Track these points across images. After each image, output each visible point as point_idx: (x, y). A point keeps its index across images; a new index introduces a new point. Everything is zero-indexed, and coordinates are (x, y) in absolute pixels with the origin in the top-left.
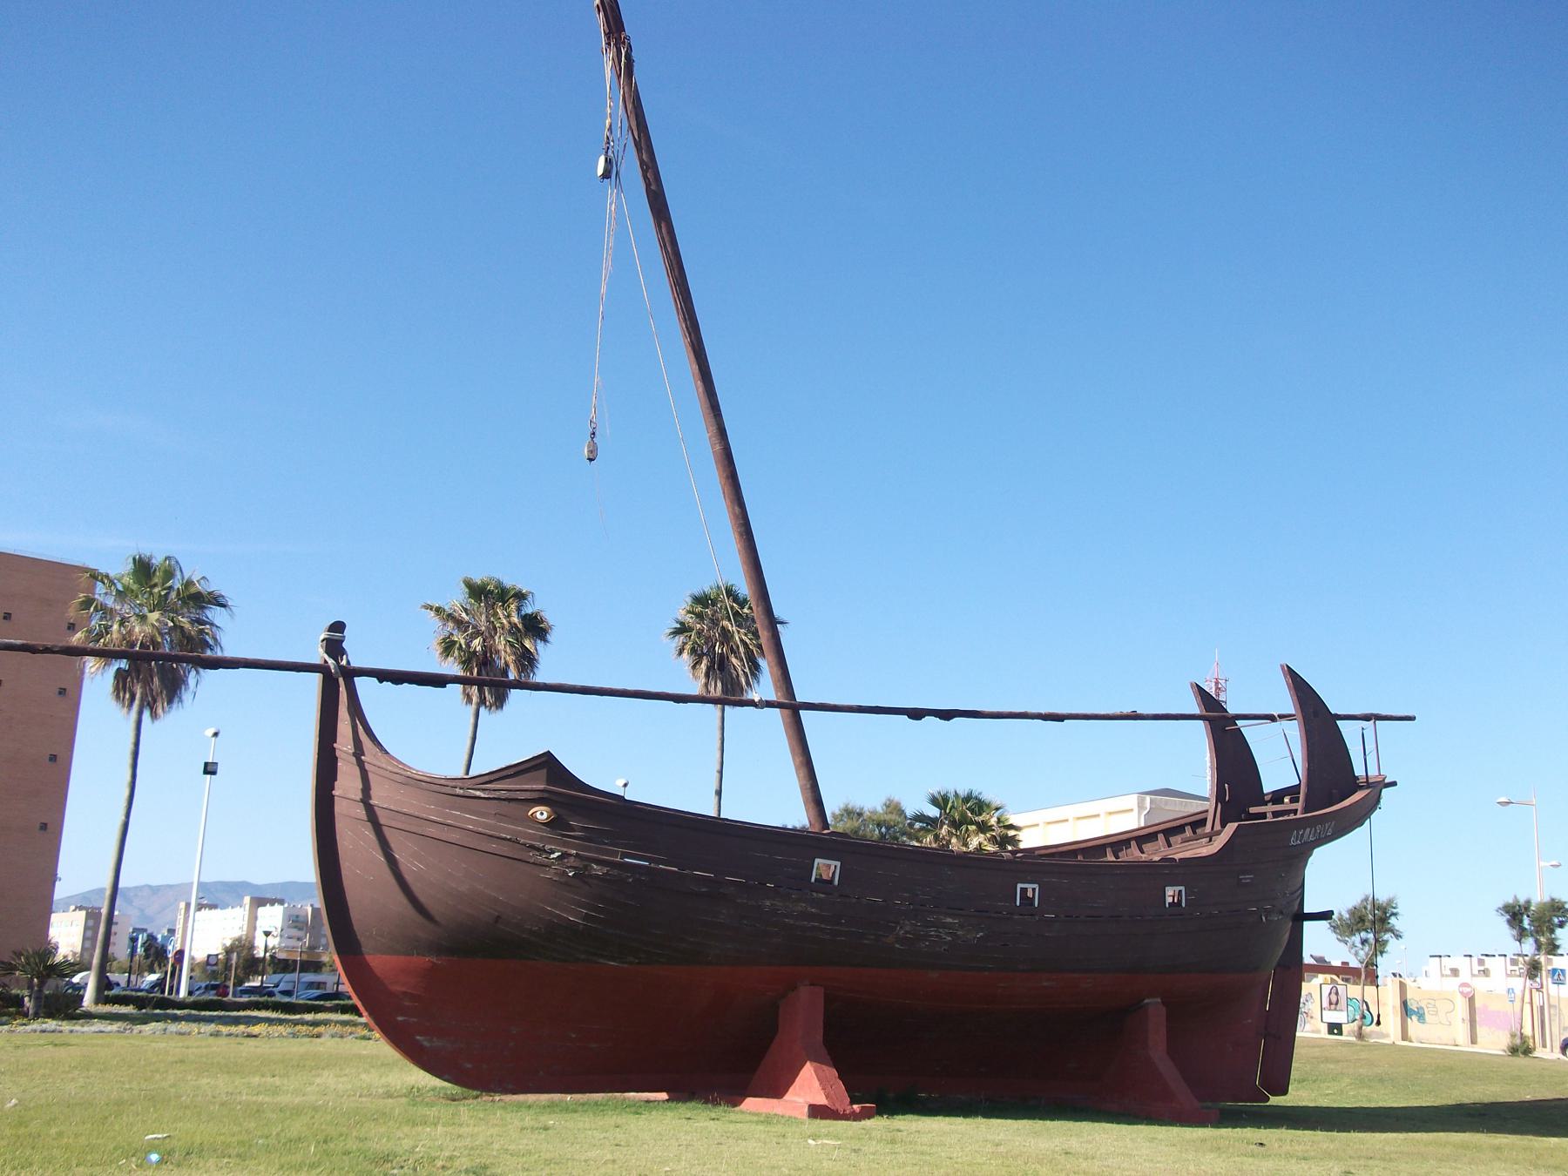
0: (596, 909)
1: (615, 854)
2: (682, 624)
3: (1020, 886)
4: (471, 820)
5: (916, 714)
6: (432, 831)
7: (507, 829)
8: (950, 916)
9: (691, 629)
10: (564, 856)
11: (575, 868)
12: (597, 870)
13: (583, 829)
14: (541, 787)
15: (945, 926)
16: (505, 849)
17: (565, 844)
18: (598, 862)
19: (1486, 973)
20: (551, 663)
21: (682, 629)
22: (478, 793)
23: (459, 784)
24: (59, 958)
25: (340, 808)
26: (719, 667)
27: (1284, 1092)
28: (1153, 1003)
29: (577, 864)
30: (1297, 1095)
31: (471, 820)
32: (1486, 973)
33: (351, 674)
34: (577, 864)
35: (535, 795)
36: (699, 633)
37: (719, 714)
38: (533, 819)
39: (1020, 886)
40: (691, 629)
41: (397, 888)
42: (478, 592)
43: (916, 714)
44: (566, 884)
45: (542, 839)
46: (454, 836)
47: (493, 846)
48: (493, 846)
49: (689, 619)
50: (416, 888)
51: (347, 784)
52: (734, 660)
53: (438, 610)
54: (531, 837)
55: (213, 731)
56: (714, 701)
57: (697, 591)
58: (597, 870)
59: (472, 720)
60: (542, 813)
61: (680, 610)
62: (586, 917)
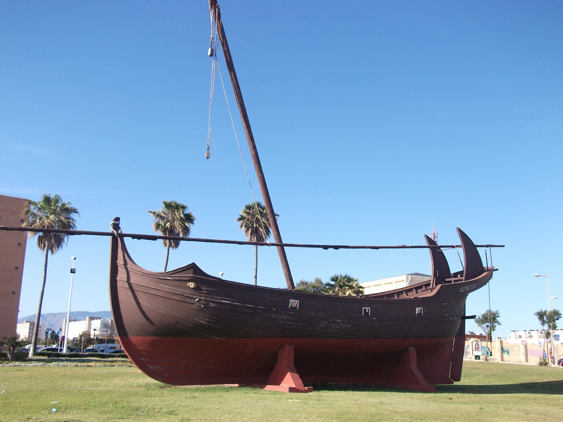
0: (213, 319)
1: (218, 299)
2: (242, 216)
4: (166, 288)
5: (326, 247)
6: (152, 292)
7: (180, 291)
8: (339, 319)
10: (200, 300)
11: (204, 304)
12: (212, 305)
15: (337, 323)
16: (178, 298)
17: (201, 296)
18: (212, 302)
19: (531, 337)
21: (242, 218)
22: (169, 278)
25: (119, 284)
26: (255, 232)
28: (412, 349)
29: (205, 303)
30: (464, 381)
31: (166, 288)
32: (531, 337)
33: (122, 236)
34: (205, 303)
35: (189, 278)
36: (248, 220)
38: (189, 287)
42: (168, 206)
43: (326, 247)
44: (200, 310)
45: (192, 294)
46: (160, 294)
47: (174, 297)
48: (174, 297)
50: (147, 313)
51: (122, 275)
53: (154, 213)
54: (188, 293)
58: (212, 305)
60: (192, 285)
62: (208, 322)
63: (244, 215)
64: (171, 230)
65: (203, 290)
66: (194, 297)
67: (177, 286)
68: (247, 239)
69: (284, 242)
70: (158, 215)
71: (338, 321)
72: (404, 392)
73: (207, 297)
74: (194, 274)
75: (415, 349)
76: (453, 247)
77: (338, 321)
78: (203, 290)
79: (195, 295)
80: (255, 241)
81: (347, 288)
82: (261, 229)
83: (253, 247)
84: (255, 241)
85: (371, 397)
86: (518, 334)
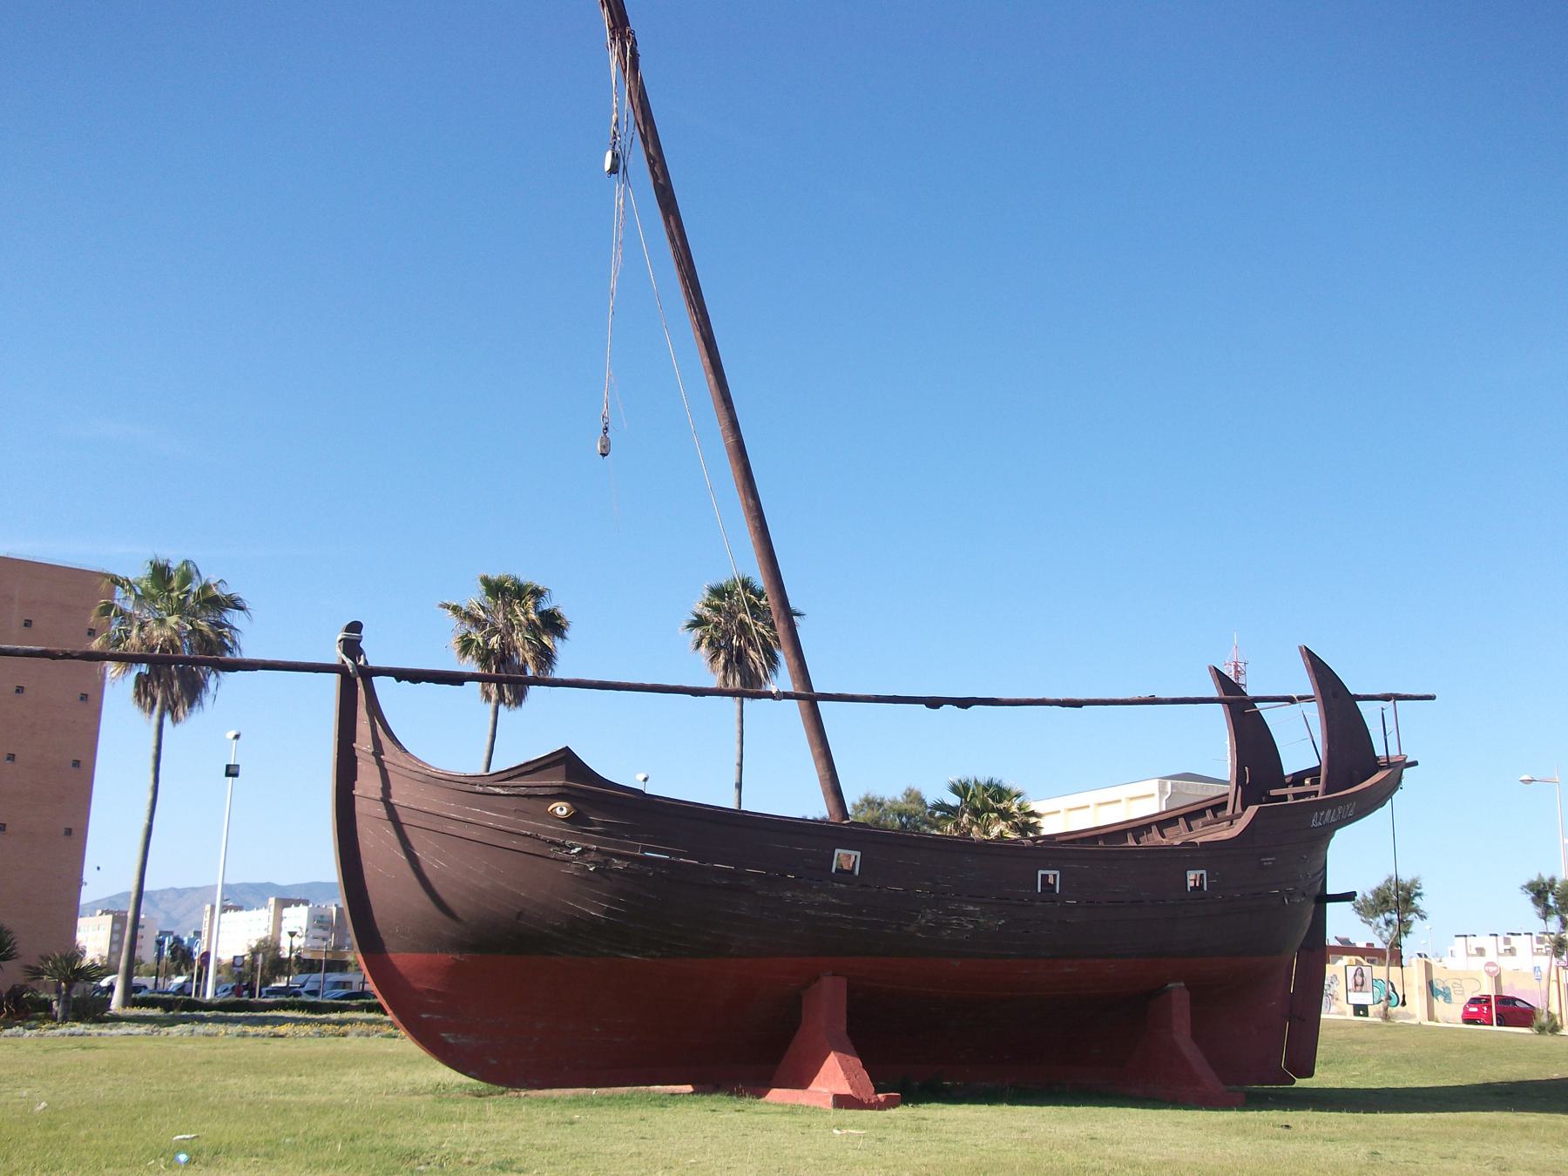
0: (619, 904)
1: (635, 848)
2: (698, 616)
4: (491, 817)
5: (934, 703)
6: (452, 828)
7: (529, 825)
8: (974, 904)
11: (595, 863)
13: (603, 824)
14: (561, 782)
15: (966, 914)
17: (586, 840)
19: (1512, 951)
20: (569, 659)
21: (699, 622)
22: (497, 790)
23: (478, 781)
24: (86, 962)
26: (737, 660)
27: (1310, 1074)
29: (599, 858)
30: (1324, 1077)
31: (491, 817)
32: (1512, 951)
33: (369, 673)
34: (599, 858)
35: (555, 791)
38: (553, 815)
42: (495, 589)
43: (934, 703)
44: (587, 879)
45: (562, 834)
46: (474, 833)
47: (514, 843)
48: (514, 843)
51: (367, 783)
52: (752, 653)
53: (456, 609)
54: (552, 833)
56: (733, 694)
57: (714, 584)
59: (491, 718)
60: (561, 809)
61: (697, 603)
62: (608, 912)
63: (707, 613)
65: (592, 824)
66: (568, 843)
68: (714, 681)
74: (568, 778)
75: (1187, 987)
76: (1291, 700)
78: (592, 824)
79: (570, 836)
80: (738, 685)
83: (731, 703)
86: (1474, 943)
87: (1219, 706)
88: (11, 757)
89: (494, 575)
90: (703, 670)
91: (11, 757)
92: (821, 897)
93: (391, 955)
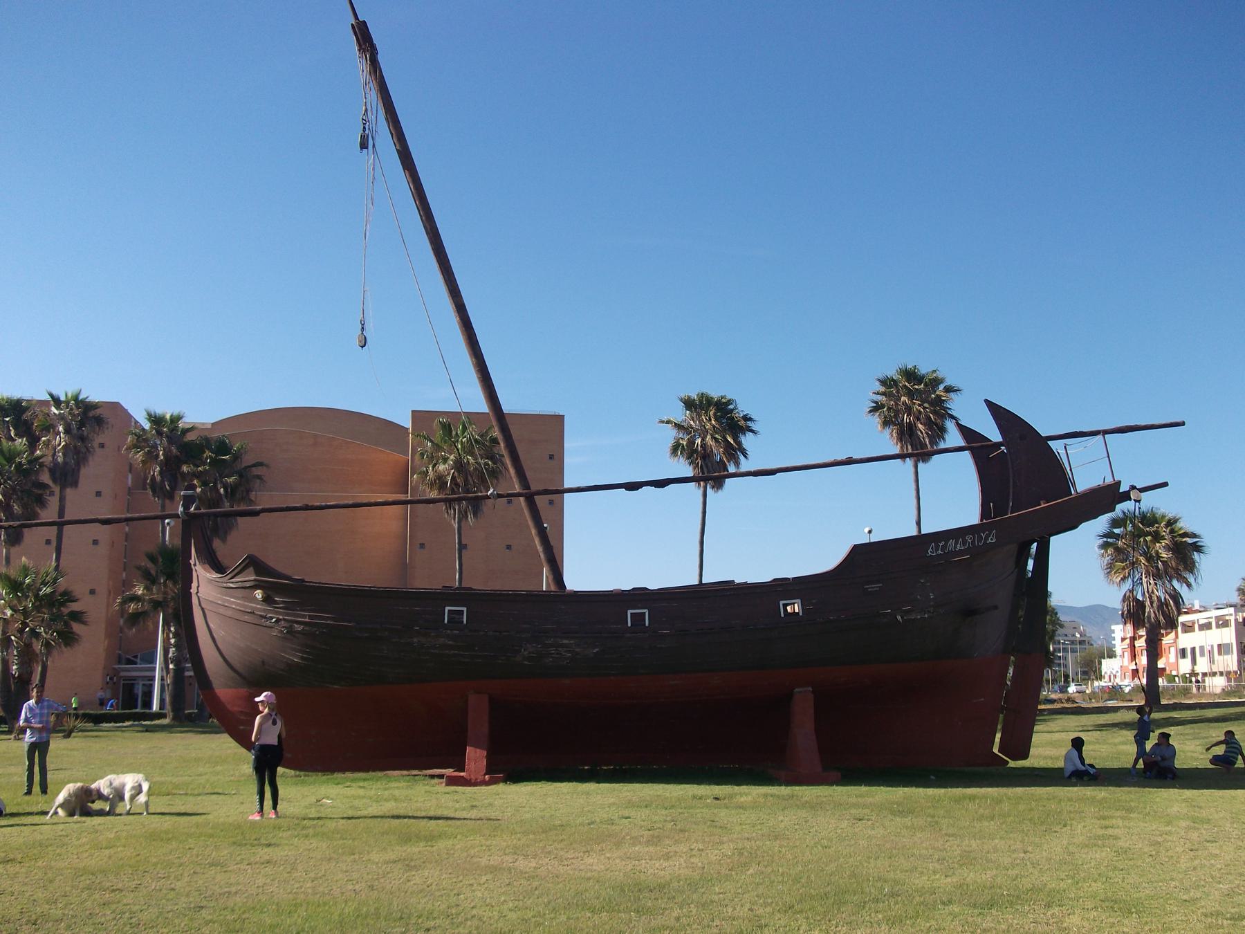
3: (465, 609)
5: (633, 486)
8: (567, 638)
9: (883, 406)
12: (299, 628)
15: (562, 646)
20: (758, 450)
21: (877, 407)
26: (906, 434)
27: (1025, 756)
29: (287, 625)
34: (287, 625)
36: (889, 409)
37: (701, 491)
39: (465, 609)
40: (883, 406)
41: (217, 654)
43: (633, 486)
45: (264, 610)
47: (246, 618)
49: (883, 399)
53: (668, 422)
55: (866, 530)
58: (299, 628)
60: (259, 594)
61: (870, 391)
63: (883, 399)
64: (706, 455)
65: (276, 603)
67: (244, 598)
69: (66, 528)
70: (678, 426)
71: (565, 641)
72: (718, 784)
73: (288, 615)
75: (813, 692)
77: (565, 641)
78: (276, 603)
80: (910, 451)
81: (1149, 538)
82: (920, 426)
83: (909, 462)
84: (910, 451)
85: (1130, 792)
87: (967, 453)
88: (509, 547)
89: (881, 377)
90: (887, 442)
91: (509, 547)
92: (442, 640)
93: (217, 691)
